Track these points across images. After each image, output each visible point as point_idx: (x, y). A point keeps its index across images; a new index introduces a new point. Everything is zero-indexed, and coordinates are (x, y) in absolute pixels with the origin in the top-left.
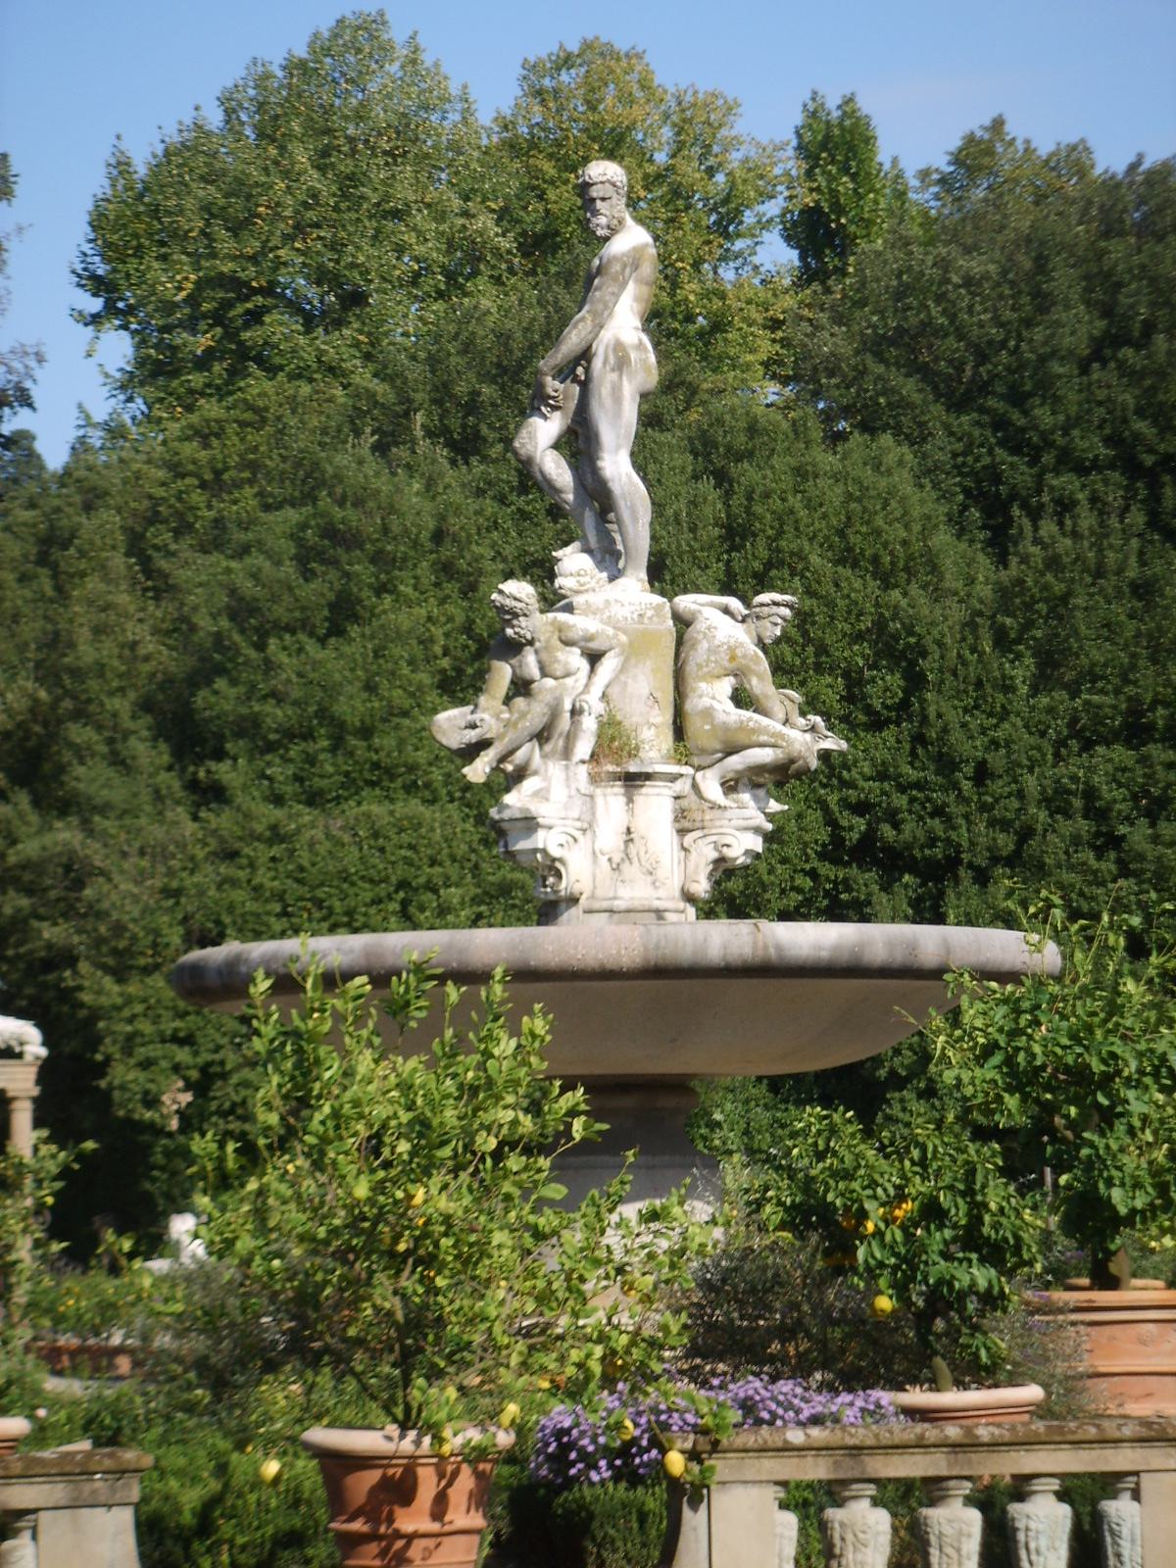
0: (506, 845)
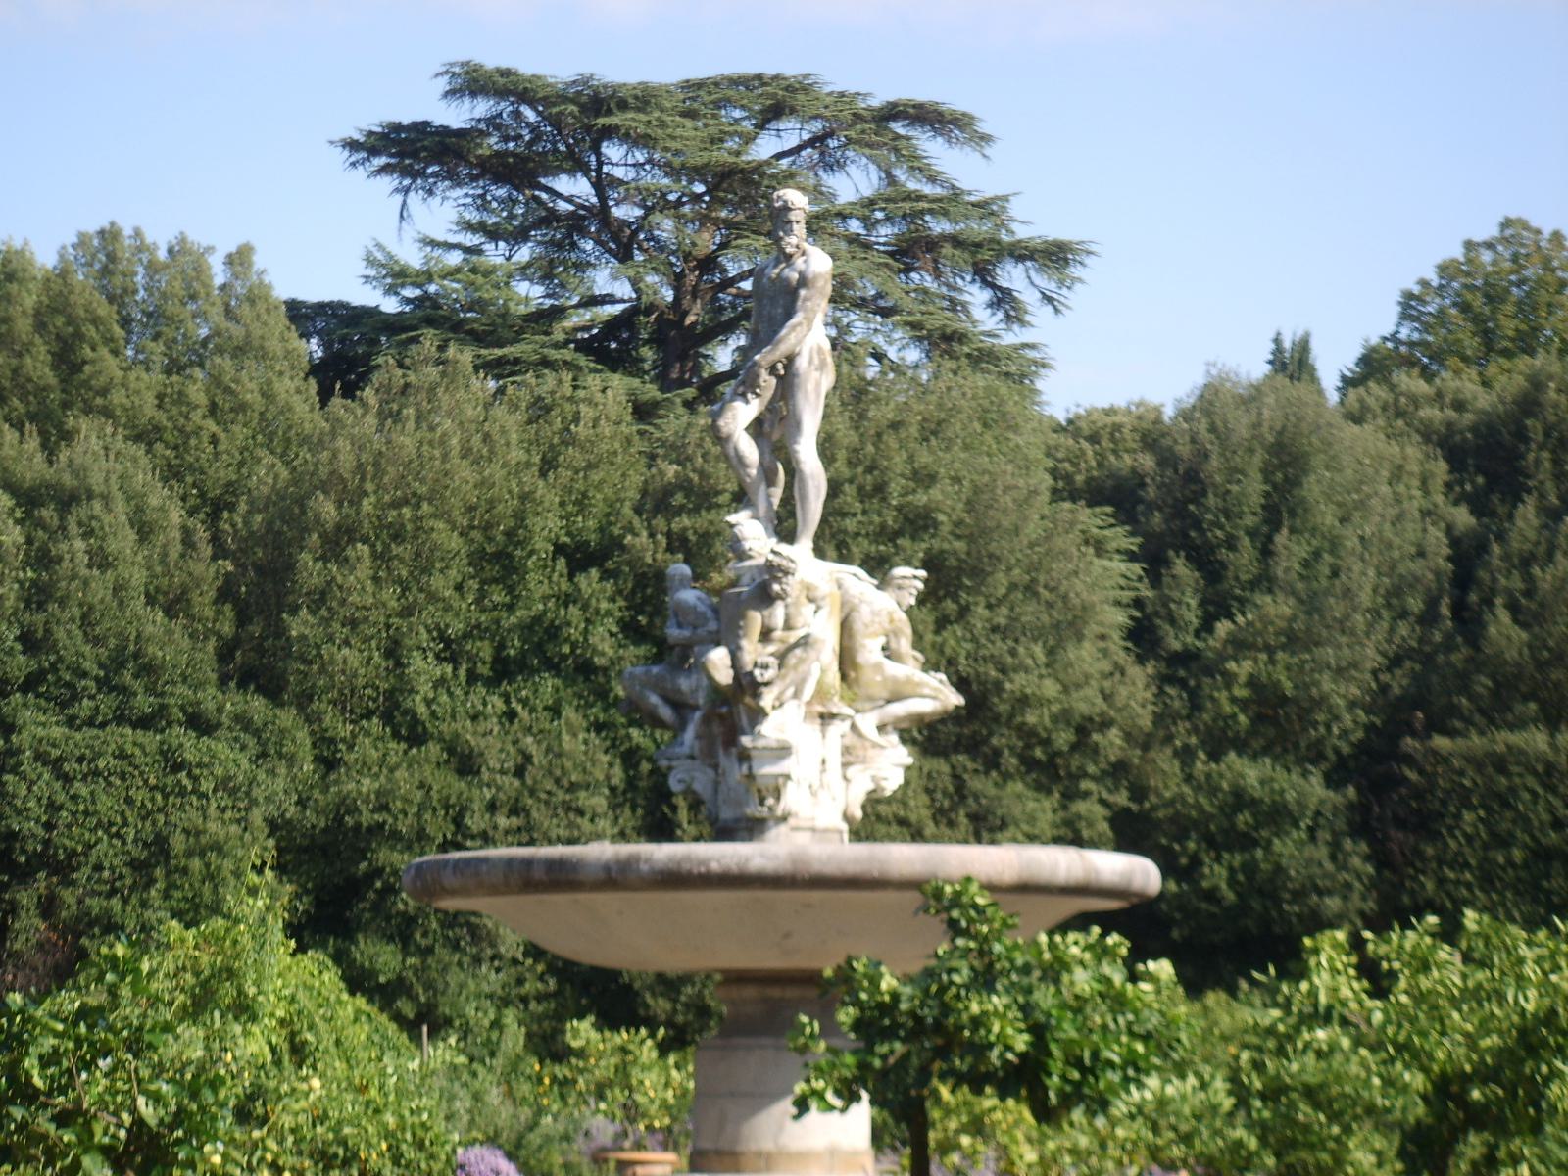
0: (750, 768)
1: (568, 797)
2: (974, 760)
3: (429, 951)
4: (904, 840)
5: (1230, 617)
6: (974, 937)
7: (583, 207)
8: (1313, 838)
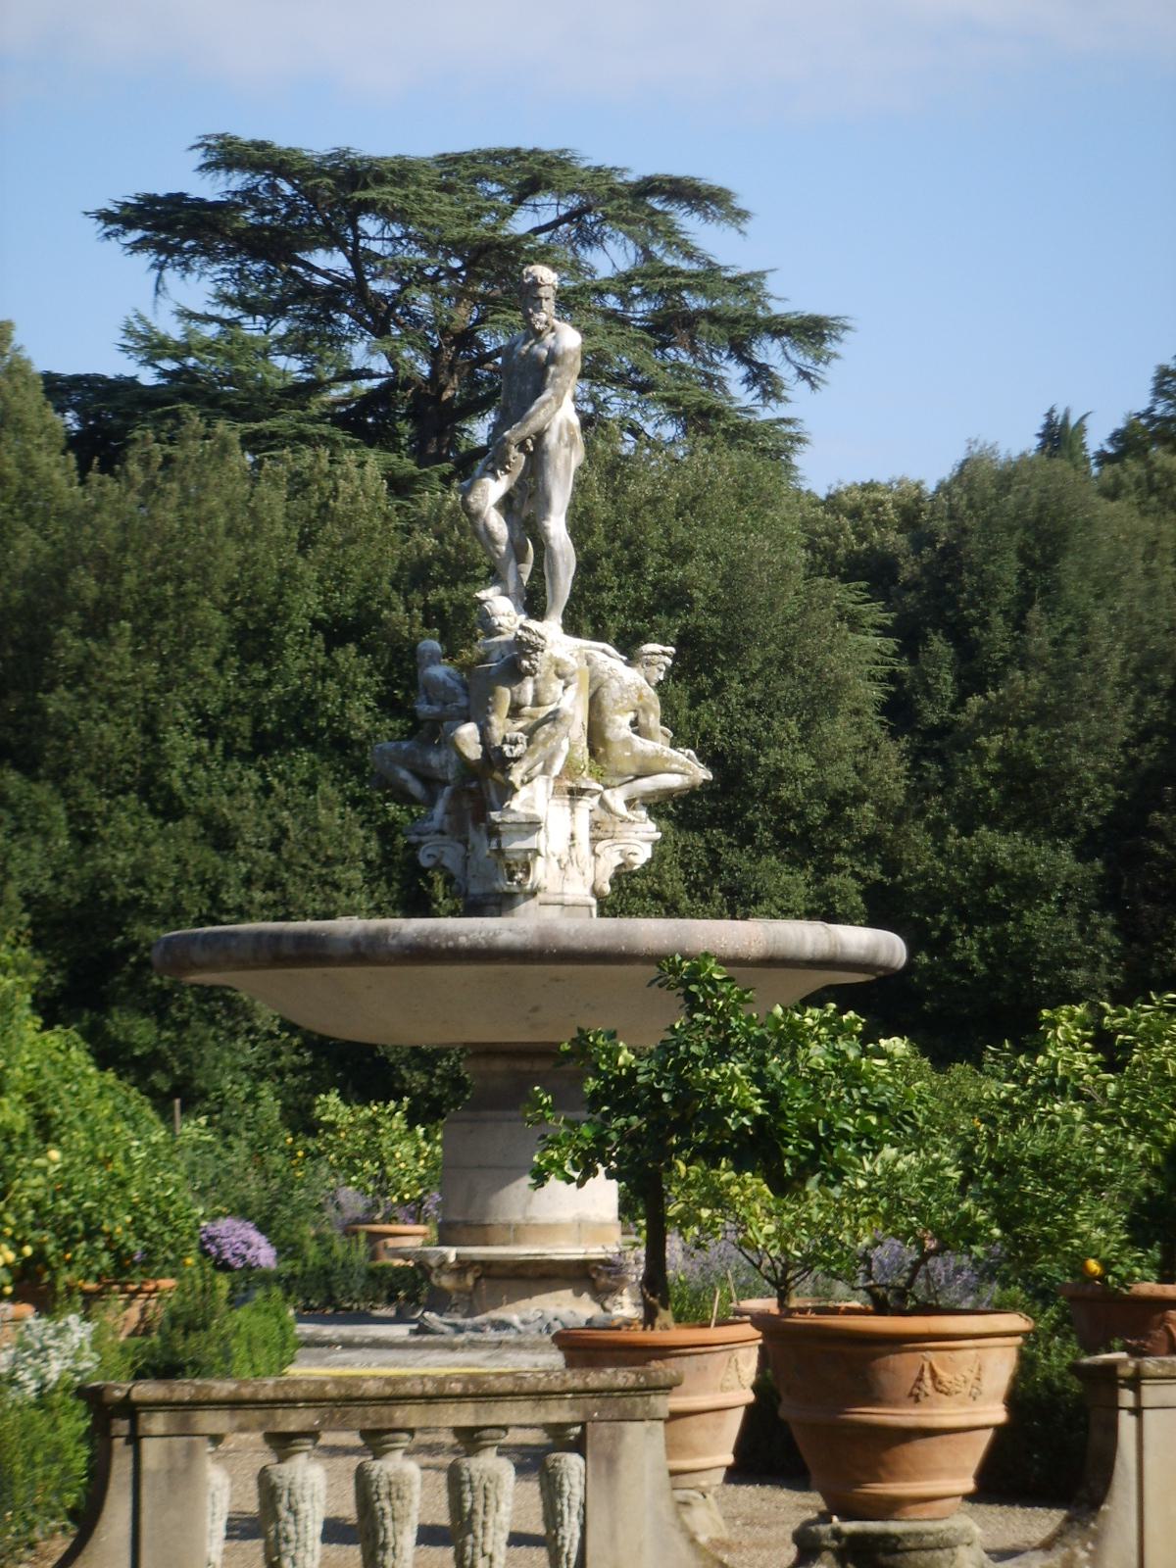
0: (499, 844)
1: (324, 871)
2: (729, 835)
3: (184, 1024)
4: (658, 915)
5: (982, 692)
6: (710, 1013)
7: (337, 281)
8: (1062, 912)
